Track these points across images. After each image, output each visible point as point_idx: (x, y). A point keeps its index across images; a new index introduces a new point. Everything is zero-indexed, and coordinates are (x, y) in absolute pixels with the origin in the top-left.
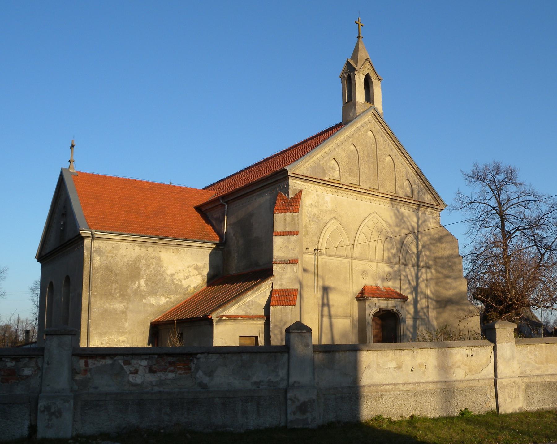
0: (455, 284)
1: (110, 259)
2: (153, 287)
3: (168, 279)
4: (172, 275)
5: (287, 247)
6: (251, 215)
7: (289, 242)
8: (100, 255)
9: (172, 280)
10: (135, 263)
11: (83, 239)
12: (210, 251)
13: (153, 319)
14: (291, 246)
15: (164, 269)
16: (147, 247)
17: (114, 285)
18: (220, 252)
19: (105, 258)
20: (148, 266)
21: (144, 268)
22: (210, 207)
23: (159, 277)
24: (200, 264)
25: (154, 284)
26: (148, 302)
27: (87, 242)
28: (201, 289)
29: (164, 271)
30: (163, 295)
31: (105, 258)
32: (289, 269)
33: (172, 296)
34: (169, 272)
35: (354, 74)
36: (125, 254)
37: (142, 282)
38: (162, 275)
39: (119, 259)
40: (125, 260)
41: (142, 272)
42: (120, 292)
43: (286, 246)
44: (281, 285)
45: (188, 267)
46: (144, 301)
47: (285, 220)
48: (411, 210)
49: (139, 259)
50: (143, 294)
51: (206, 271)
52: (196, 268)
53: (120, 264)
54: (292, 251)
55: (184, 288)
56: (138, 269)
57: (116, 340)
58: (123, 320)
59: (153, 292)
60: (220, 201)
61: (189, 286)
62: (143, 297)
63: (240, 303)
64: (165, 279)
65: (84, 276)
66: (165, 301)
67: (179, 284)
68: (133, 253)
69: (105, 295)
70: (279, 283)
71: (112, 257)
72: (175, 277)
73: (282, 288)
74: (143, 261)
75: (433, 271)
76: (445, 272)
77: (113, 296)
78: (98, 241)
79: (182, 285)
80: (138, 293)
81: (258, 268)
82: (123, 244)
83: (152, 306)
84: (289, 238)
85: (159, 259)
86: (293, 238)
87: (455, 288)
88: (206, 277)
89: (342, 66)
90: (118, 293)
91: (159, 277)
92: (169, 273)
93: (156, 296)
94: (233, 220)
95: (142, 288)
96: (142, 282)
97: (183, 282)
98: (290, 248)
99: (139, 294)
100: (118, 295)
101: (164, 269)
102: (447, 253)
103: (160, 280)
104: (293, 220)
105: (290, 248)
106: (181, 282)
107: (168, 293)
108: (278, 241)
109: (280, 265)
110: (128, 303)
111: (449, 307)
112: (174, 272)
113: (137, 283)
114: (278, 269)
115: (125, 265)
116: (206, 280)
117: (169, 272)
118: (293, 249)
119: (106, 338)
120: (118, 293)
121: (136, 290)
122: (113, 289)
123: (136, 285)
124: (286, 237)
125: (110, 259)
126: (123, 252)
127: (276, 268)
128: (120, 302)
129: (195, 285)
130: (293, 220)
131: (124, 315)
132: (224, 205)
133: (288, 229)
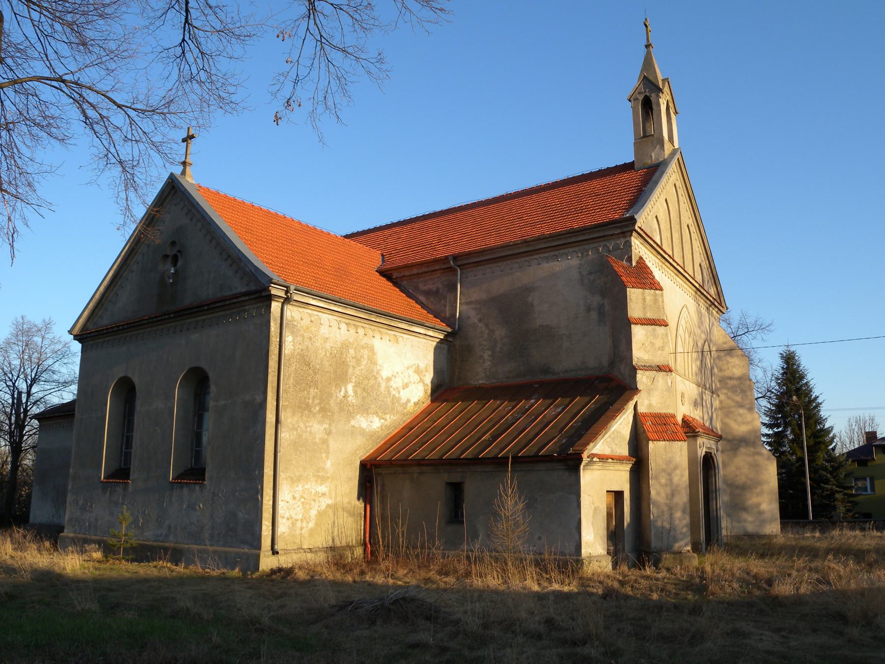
0: (749, 417)
1: (307, 343)
2: (364, 398)
3: (383, 385)
4: (388, 379)
5: (652, 344)
6: (528, 289)
7: (655, 336)
8: (292, 333)
9: (388, 388)
10: (341, 353)
11: (270, 298)
12: (435, 344)
13: (363, 454)
14: (658, 343)
15: (378, 367)
16: (356, 327)
17: (312, 390)
18: (445, 346)
19: (299, 339)
20: (358, 361)
21: (352, 363)
22: (415, 271)
23: (372, 382)
24: (422, 366)
25: (365, 394)
26: (357, 425)
27: (275, 306)
28: (423, 406)
29: (378, 373)
30: (376, 413)
31: (299, 339)
32: (660, 380)
33: (388, 416)
34: (385, 374)
35: (658, 97)
36: (327, 336)
37: (350, 388)
38: (376, 378)
39: (319, 344)
40: (328, 346)
41: (350, 371)
42: (320, 404)
43: (651, 343)
44: (650, 406)
45: (408, 368)
46: (353, 423)
47: (644, 299)
48: (10, 337)
49: (345, 346)
50: (351, 409)
51: (429, 376)
52: (418, 371)
53: (322, 353)
54: (660, 352)
55: (403, 404)
56: (344, 363)
57: (314, 492)
58: (324, 455)
59: (364, 409)
60: (449, 262)
61: (408, 401)
62: (350, 415)
63: (606, 436)
64: (379, 386)
65: (270, 370)
66: (379, 425)
67: (397, 395)
68: (338, 336)
69: (299, 407)
70: (646, 402)
71: (311, 339)
72: (392, 383)
73: (651, 411)
74: (352, 351)
75: (722, 397)
76: (738, 399)
77: (310, 411)
78: (295, 309)
79: (400, 398)
80: (343, 405)
81: (549, 377)
82: (325, 317)
83: (362, 432)
84: (654, 330)
85: (372, 350)
86: (660, 330)
87: (748, 423)
88: (430, 385)
89: (632, 82)
90: (316, 405)
91: (372, 382)
92: (384, 377)
93: (368, 414)
94: (477, 294)
95: (350, 399)
96: (350, 388)
97: (402, 392)
98: (657, 346)
99: (347, 410)
100: (317, 408)
101: (378, 367)
102: (737, 372)
103: (372, 386)
104: (656, 301)
105: (657, 346)
106: (399, 393)
107: (382, 411)
108: (638, 333)
109: (647, 373)
110: (330, 425)
111: (743, 450)
112: (390, 376)
113: (343, 389)
114: (644, 379)
115: (328, 355)
116: (429, 391)
117: (385, 374)
118: (662, 348)
119: (300, 488)
120: (316, 405)
121: (341, 402)
122: (311, 397)
123: (342, 393)
124: (650, 328)
125: (307, 343)
126: (324, 331)
127: (642, 378)
128: (321, 423)
129: (416, 400)
130: (656, 301)
131: (325, 446)
132: (456, 270)
133: (649, 315)
